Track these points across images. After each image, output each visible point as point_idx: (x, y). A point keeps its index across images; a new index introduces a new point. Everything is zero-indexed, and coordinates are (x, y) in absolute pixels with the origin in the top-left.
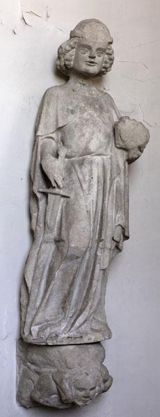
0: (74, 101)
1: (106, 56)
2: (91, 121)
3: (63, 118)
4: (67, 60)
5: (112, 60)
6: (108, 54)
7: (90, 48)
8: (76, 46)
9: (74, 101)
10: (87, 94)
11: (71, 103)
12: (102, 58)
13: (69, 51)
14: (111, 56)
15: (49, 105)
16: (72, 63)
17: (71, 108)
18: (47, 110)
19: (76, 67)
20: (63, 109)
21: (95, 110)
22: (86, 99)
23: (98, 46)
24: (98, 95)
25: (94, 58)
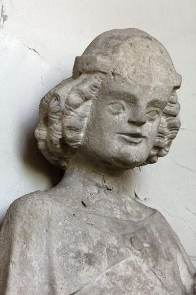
0: (92, 231)
1: (163, 119)
2: (136, 284)
3: (67, 276)
4: (70, 128)
5: (174, 128)
6: (168, 114)
7: (132, 101)
8: (94, 94)
9: (92, 231)
10: (118, 214)
11: (85, 235)
12: (155, 123)
13: (77, 106)
14: (175, 120)
15: (26, 239)
16: (82, 135)
17: (85, 249)
18: (23, 254)
19: (95, 145)
20: (64, 251)
21: (144, 256)
22: (117, 225)
23: (151, 96)
24: (139, 216)
25: (140, 124)
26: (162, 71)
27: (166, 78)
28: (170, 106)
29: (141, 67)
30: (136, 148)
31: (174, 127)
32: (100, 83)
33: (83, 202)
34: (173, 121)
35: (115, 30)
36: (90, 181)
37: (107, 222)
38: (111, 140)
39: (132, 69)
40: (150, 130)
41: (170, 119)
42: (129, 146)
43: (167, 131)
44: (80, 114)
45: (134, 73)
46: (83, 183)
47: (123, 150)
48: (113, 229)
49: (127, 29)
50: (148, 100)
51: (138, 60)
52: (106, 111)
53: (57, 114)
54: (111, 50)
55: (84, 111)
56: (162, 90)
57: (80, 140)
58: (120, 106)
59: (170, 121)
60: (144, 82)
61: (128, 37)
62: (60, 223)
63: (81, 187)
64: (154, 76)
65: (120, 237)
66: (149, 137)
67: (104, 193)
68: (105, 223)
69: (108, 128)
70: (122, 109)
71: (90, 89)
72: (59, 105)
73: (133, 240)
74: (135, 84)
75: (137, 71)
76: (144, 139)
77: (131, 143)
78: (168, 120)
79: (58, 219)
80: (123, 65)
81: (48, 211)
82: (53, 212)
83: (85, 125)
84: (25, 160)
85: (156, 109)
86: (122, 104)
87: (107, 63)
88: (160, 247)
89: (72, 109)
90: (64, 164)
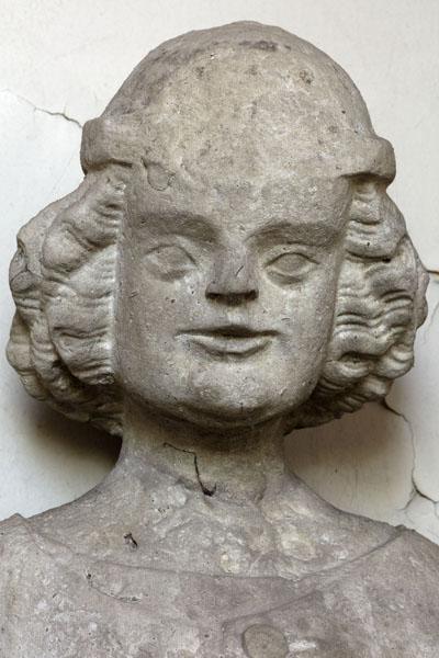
1: (353, 272)
7: (205, 233)
13: (70, 268)
14: (394, 270)
16: (107, 345)
22: (217, 591)
23: (259, 213)
26: (294, 136)
27: (307, 154)
28: (364, 232)
29: (225, 133)
30: (246, 367)
31: (391, 292)
32: (121, 193)
33: (129, 536)
34: (385, 275)
35: (165, 43)
36: (163, 472)
37: (183, 590)
38: (164, 354)
39: (198, 144)
40: (288, 309)
41: (377, 270)
42: (220, 366)
43: (372, 304)
44: (83, 290)
45: (204, 153)
46: (143, 481)
47: (200, 379)
48: (197, 608)
49: (181, 37)
50: (252, 227)
51: (218, 116)
52: (144, 272)
53: (30, 294)
54: (144, 95)
55: (97, 277)
56: (294, 191)
57: (108, 362)
58: (179, 252)
59: (377, 274)
60: (230, 177)
61: (198, 51)
62: (42, 605)
63: (136, 493)
64: (263, 155)
65: (216, 629)
66: (290, 331)
67: (201, 503)
68: (176, 592)
69: (154, 321)
70: (189, 261)
71: (97, 215)
72: (27, 269)
73: (247, 636)
74: (203, 186)
75: (214, 148)
76: (274, 340)
77: (222, 355)
78: (369, 275)
79: (36, 592)
80: (172, 136)
81: (10, 573)
82: (25, 574)
83: (111, 317)
84: (39, 427)
85: (293, 248)
86: (183, 245)
87: (129, 134)
88: (363, 646)
89: (58, 276)
90: (115, 430)
